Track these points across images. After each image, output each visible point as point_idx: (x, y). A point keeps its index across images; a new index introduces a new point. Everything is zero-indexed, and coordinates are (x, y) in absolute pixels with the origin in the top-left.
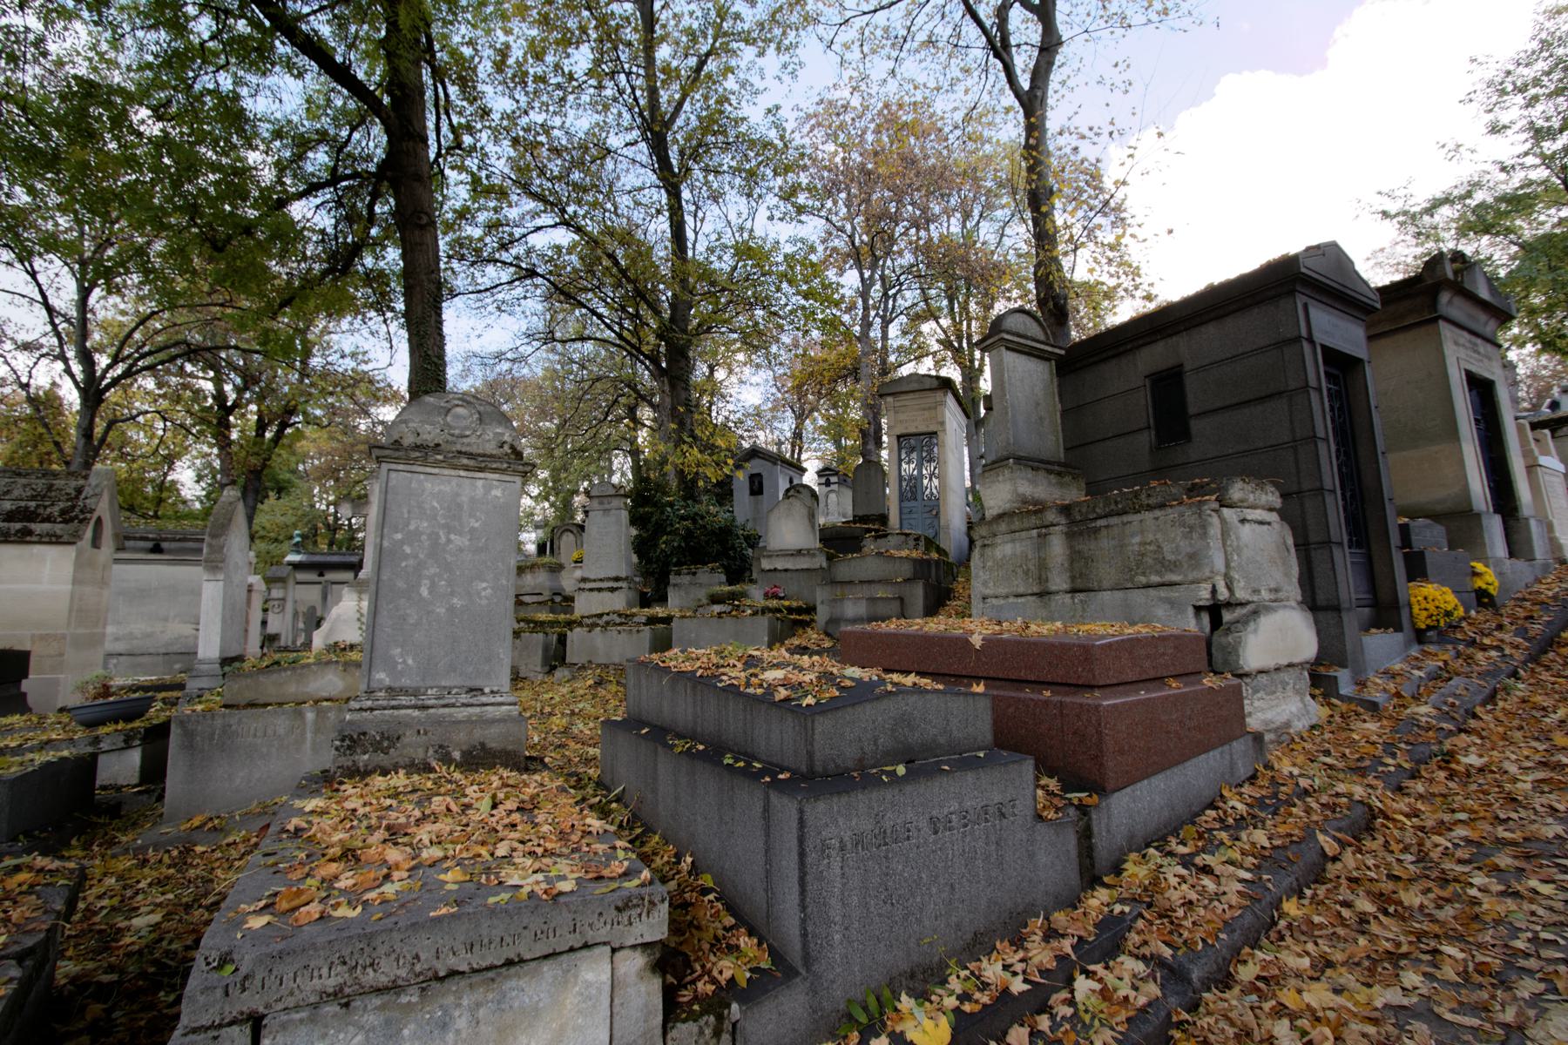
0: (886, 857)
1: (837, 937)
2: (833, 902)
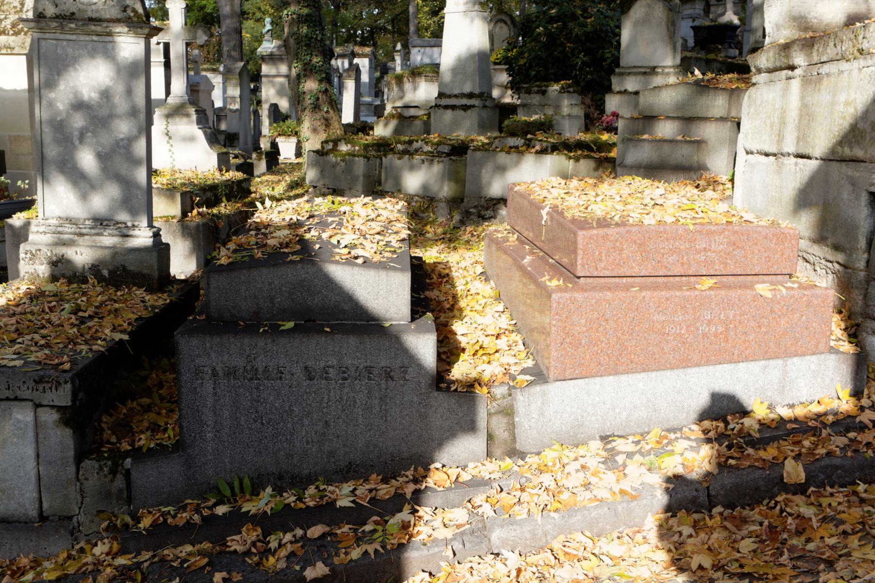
0: (257, 389)
1: (209, 435)
2: (206, 410)
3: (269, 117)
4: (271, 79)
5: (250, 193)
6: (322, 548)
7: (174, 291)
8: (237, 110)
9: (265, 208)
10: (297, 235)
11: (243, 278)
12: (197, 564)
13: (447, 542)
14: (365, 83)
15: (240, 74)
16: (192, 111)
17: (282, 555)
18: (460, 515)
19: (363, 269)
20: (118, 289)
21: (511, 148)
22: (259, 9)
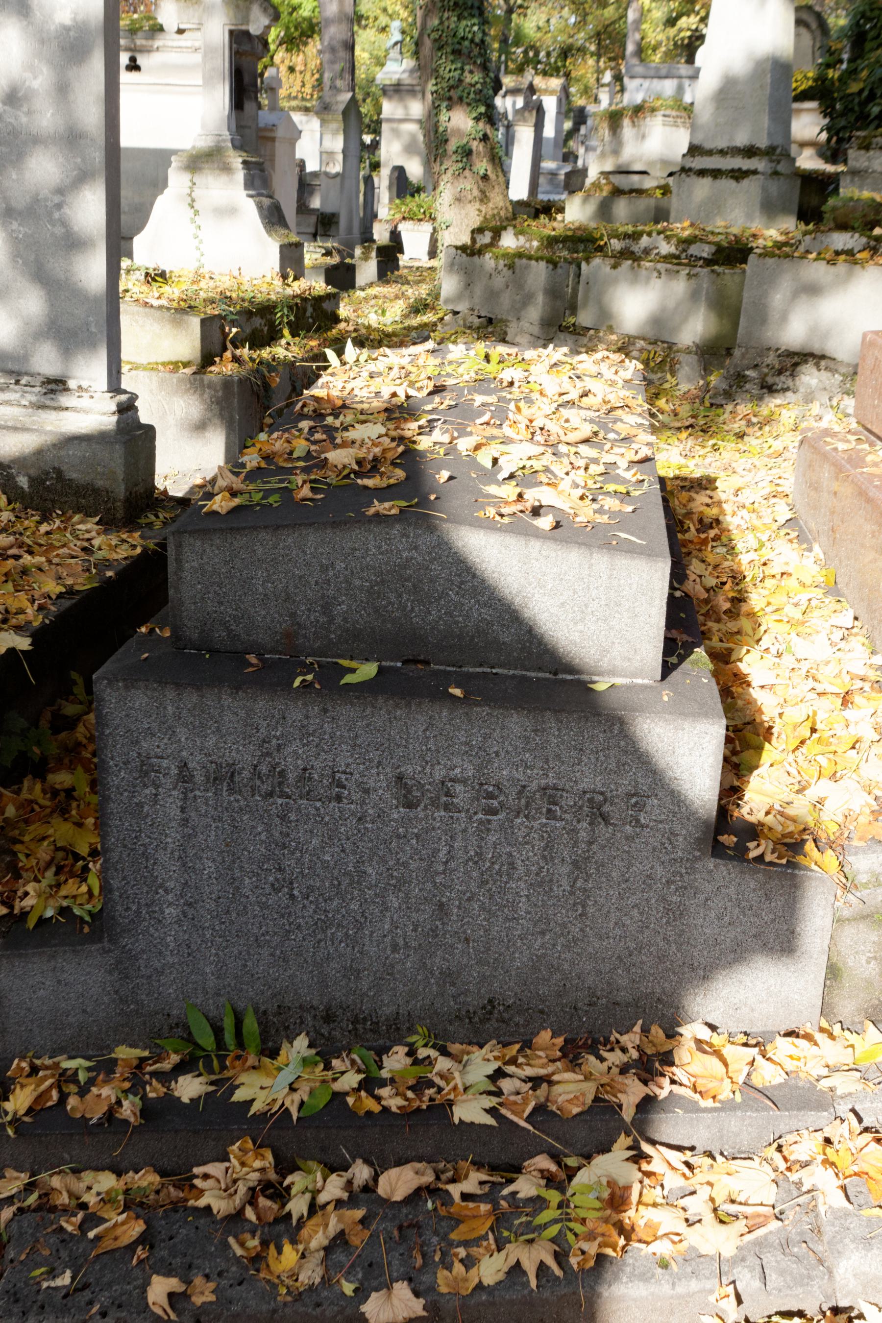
0: (283, 818)
1: (171, 912)
2: (163, 857)
3: (390, 187)
4: (395, 125)
5: (336, 320)
6: (406, 1239)
7: (158, 525)
8: (337, 175)
9: (344, 363)
10: (401, 439)
11: (260, 551)
12: (119, 1231)
13: (721, 1267)
14: (548, 139)
15: (345, 113)
16: (236, 161)
17: (314, 1244)
18: (753, 1183)
19: (550, 545)
20: (45, 518)
21: (837, 253)
22: (385, 10)
